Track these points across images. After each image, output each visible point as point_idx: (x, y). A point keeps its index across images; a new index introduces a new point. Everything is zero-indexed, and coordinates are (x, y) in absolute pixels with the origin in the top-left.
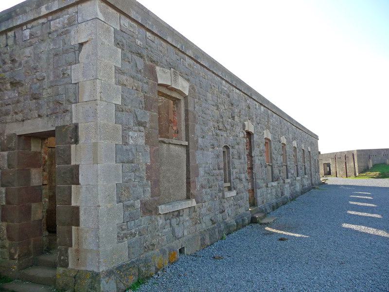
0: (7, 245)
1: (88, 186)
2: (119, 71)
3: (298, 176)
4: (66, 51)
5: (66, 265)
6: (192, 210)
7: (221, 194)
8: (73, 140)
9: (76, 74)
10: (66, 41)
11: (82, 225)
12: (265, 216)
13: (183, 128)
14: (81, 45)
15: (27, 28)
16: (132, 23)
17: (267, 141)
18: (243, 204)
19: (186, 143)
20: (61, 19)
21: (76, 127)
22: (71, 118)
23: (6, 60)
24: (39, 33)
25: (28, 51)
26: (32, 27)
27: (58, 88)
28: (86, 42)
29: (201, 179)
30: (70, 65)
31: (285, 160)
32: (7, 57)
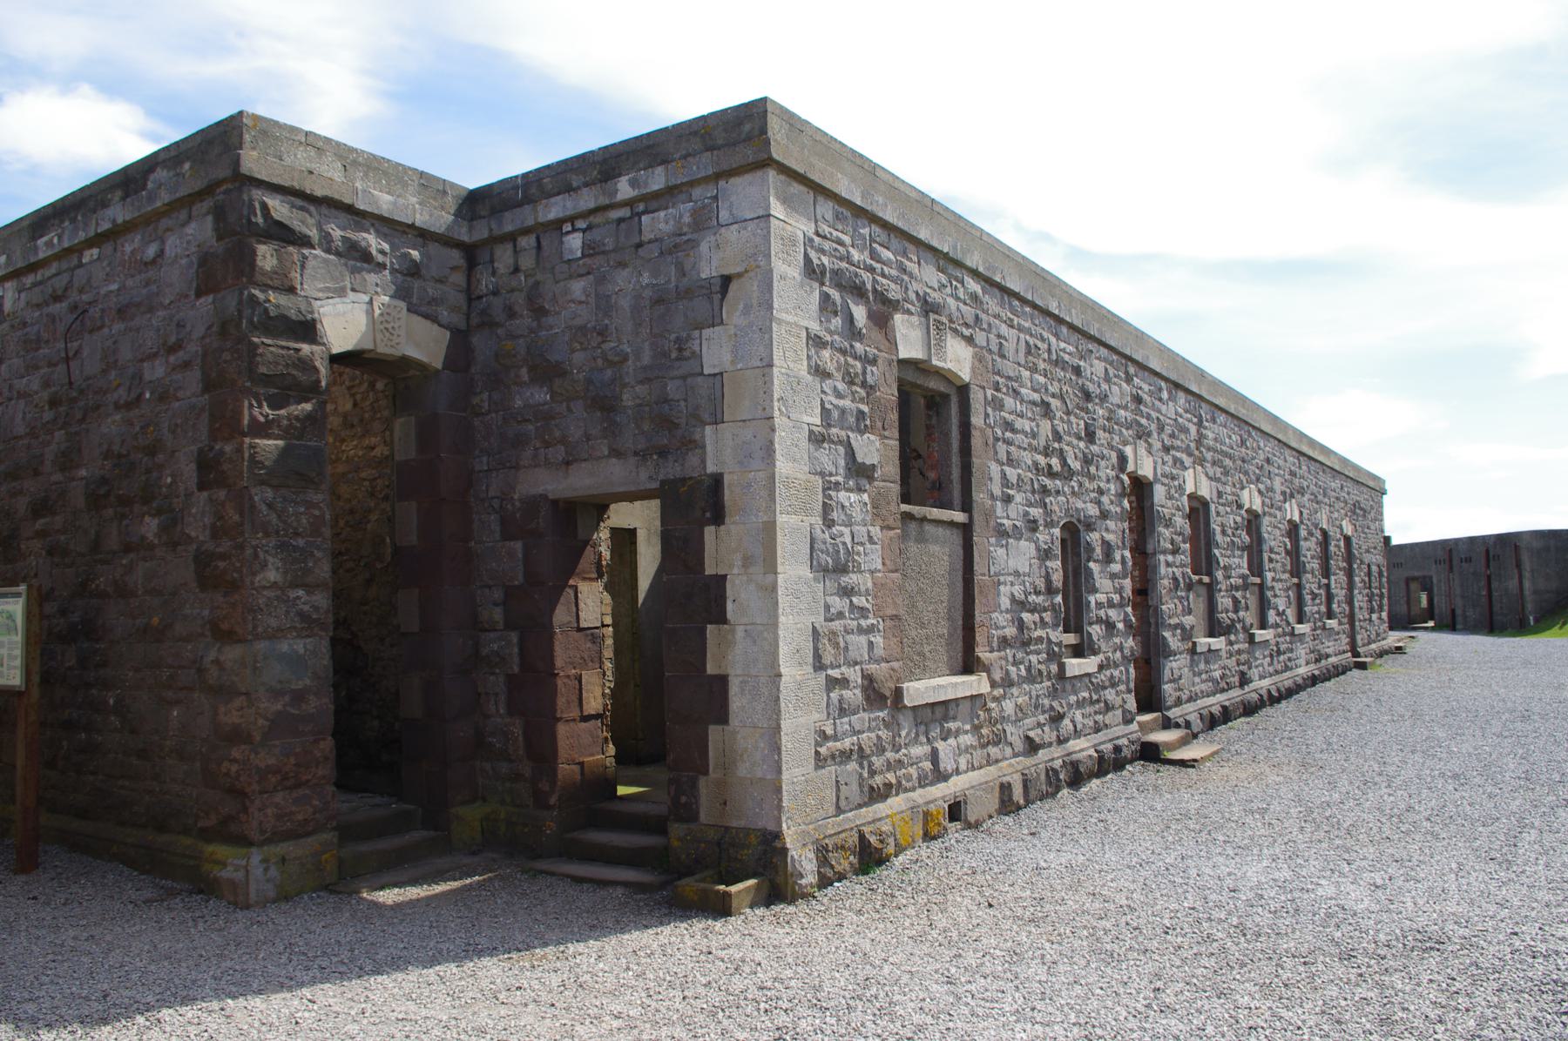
0: (527, 772)
1: (749, 627)
2: (816, 342)
3: (1300, 622)
4: (686, 294)
5: (693, 817)
6: (978, 703)
7: (1054, 668)
8: (708, 515)
9: (715, 351)
10: (687, 267)
11: (734, 721)
12: (1184, 742)
13: (956, 473)
14: (726, 280)
15: (574, 230)
16: (840, 210)
17: (1196, 504)
18: (1118, 701)
19: (959, 517)
20: (670, 210)
21: (717, 480)
22: (703, 461)
23: (517, 308)
24: (610, 243)
25: (578, 287)
26: (590, 228)
27: (666, 385)
28: (739, 275)
29: (996, 620)
30: (696, 329)
31: (1256, 567)
32: (519, 299)
